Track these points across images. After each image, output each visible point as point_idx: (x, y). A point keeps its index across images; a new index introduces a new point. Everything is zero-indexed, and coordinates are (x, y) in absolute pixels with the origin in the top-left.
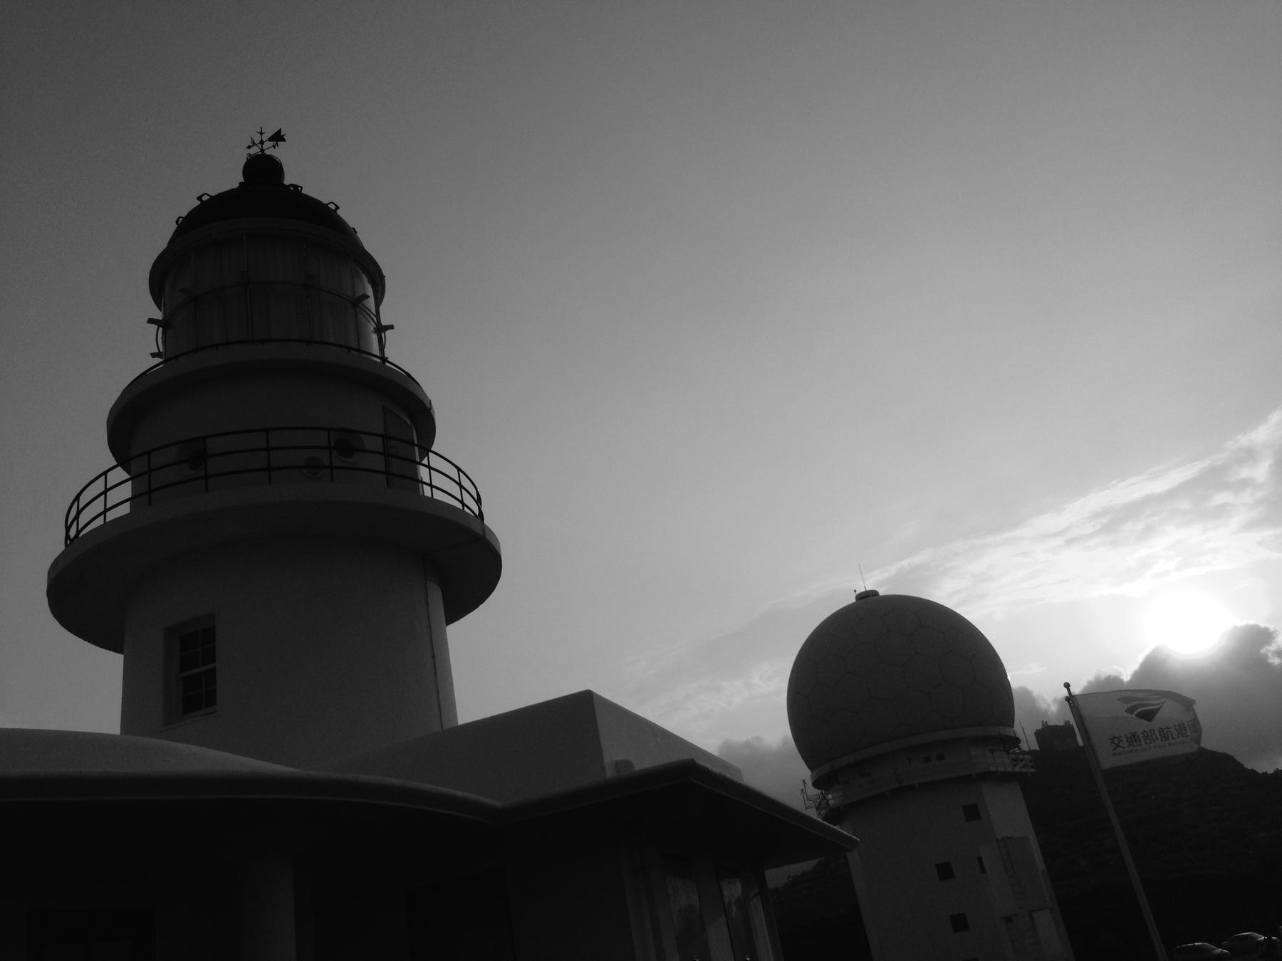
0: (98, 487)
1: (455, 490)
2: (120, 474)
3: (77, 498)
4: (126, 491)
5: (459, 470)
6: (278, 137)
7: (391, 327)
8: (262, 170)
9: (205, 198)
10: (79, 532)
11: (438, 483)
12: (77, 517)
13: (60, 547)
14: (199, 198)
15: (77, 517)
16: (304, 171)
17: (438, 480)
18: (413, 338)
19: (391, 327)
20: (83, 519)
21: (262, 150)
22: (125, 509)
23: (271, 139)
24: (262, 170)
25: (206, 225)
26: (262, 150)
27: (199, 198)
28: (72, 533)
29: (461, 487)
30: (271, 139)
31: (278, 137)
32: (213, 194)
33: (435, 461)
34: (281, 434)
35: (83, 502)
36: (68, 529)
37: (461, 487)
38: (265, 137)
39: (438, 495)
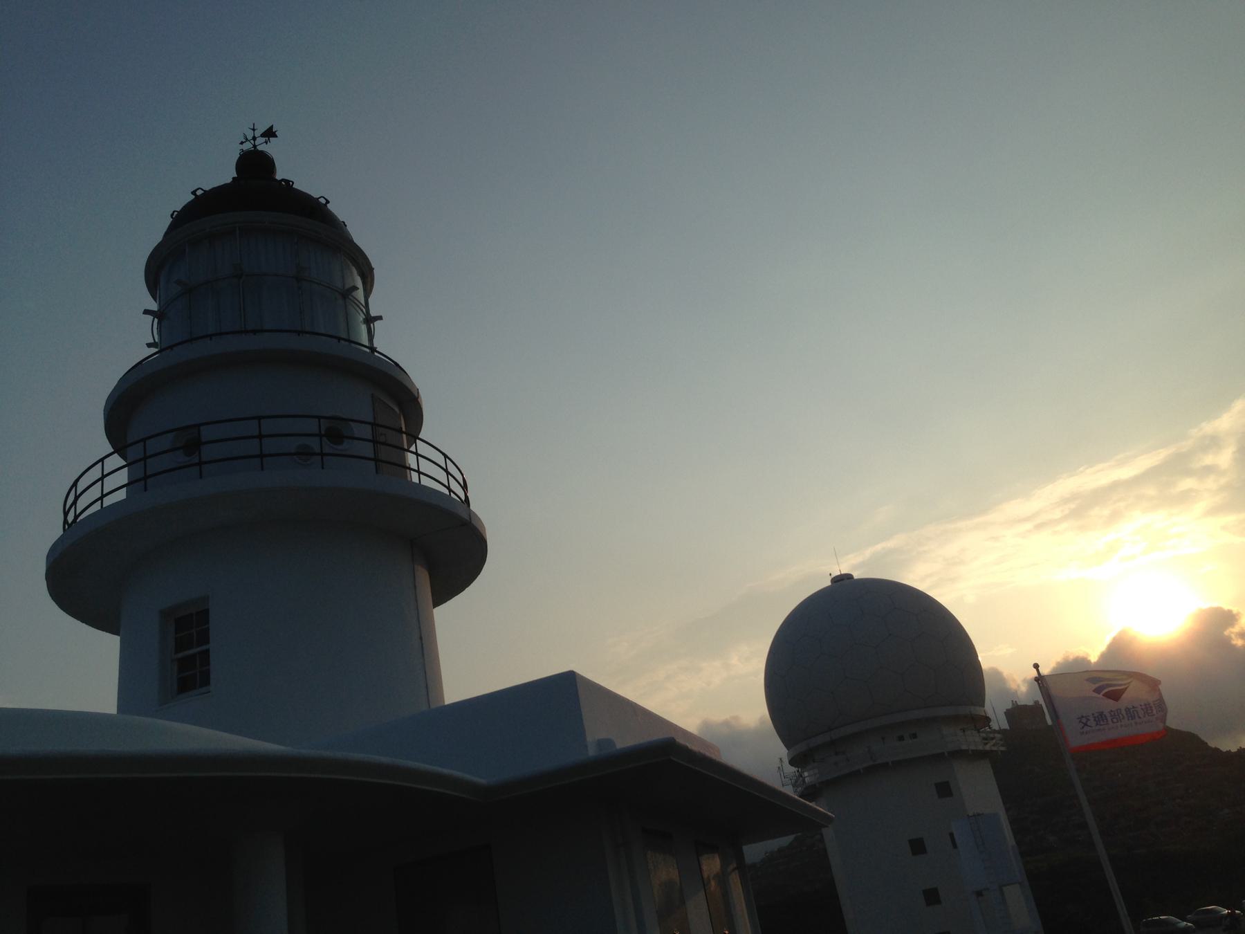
0: (96, 473)
1: (442, 476)
2: (116, 461)
3: (75, 484)
4: (122, 477)
5: (446, 456)
6: (270, 133)
7: (380, 318)
8: (255, 165)
9: (199, 193)
10: (76, 517)
11: (425, 470)
12: (75, 503)
13: (58, 532)
14: (194, 193)
15: (75, 503)
16: (295, 167)
17: (425, 466)
18: (401, 329)
19: (380, 318)
20: (81, 504)
21: (255, 146)
22: (121, 495)
23: (263, 135)
24: (255, 165)
25: (201, 218)
26: (255, 146)
27: (194, 193)
28: (70, 518)
29: (448, 473)
30: (263, 135)
31: (270, 133)
32: (207, 188)
33: (422, 448)
34: (272, 417)
35: (80, 488)
36: (66, 514)
37: (448, 473)
38: (258, 134)
39: (425, 481)
